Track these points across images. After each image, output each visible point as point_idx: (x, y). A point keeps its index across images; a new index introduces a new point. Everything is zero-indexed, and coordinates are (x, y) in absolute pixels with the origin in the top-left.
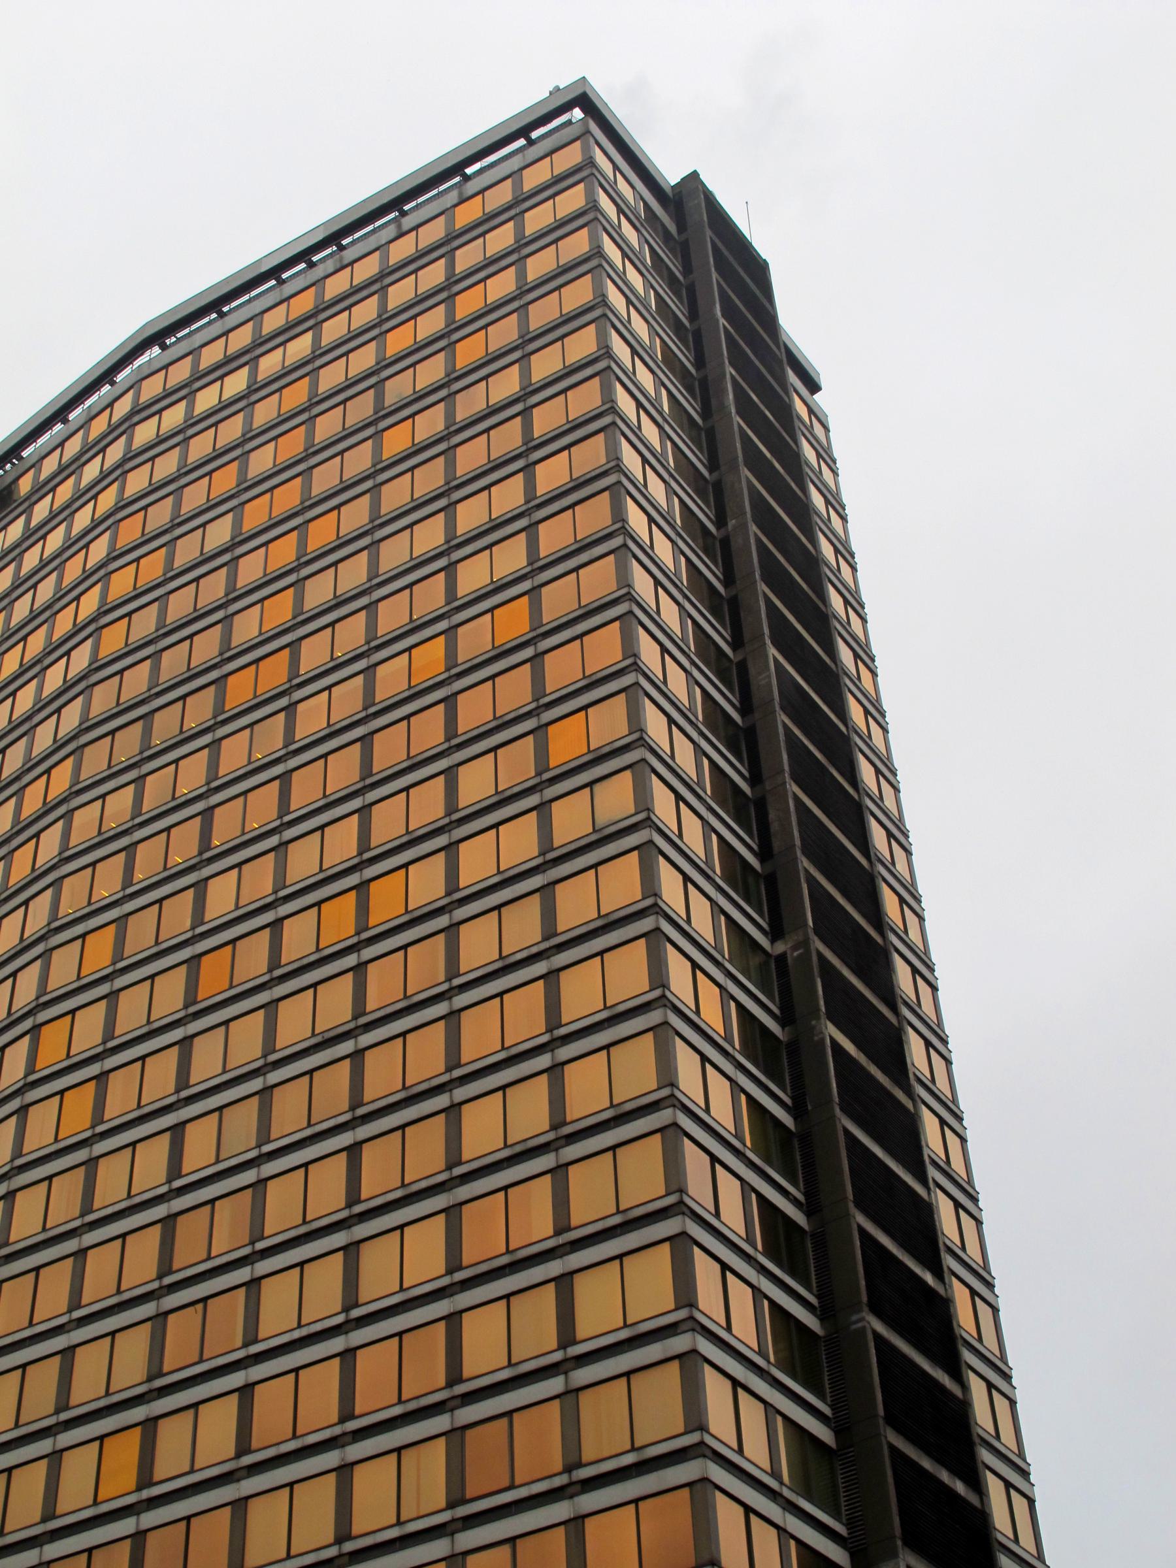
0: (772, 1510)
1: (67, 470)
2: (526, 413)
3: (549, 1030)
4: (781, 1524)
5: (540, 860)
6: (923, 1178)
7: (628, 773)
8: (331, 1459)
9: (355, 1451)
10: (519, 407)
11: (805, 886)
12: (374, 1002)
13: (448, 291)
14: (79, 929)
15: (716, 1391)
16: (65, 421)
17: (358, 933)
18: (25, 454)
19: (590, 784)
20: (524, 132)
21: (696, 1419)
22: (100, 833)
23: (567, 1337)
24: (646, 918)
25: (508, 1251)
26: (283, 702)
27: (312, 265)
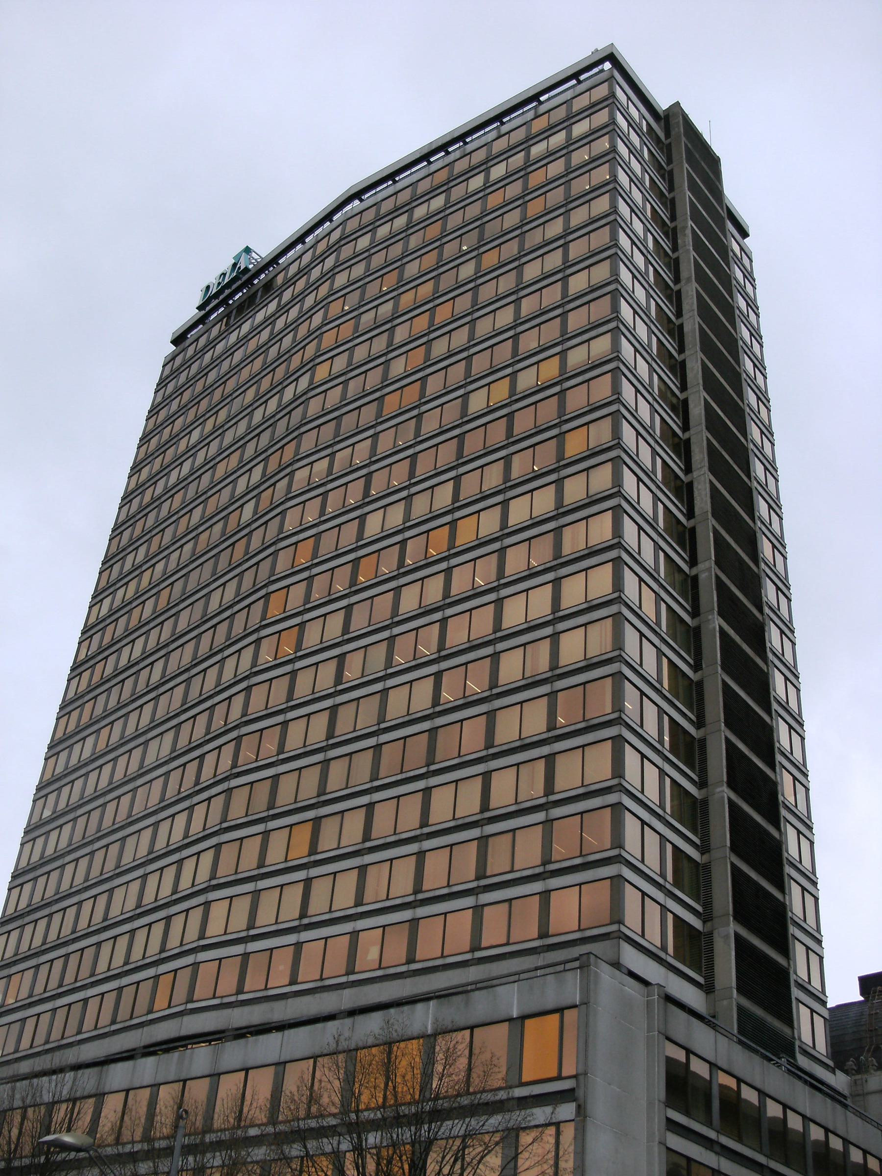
0: (659, 896)
1: (304, 271)
2: (565, 246)
3: (553, 613)
4: (663, 903)
5: (555, 513)
6: (769, 713)
7: (610, 464)
8: (414, 848)
9: (427, 844)
10: (561, 242)
11: (711, 535)
12: (567, 549)
13: (525, 171)
14: (294, 539)
15: (631, 827)
16: (304, 243)
17: (449, 550)
18: (280, 261)
19: (587, 469)
20: (576, 76)
21: (618, 841)
22: (309, 484)
23: (549, 789)
24: (613, 550)
25: (520, 739)
26: (415, 412)
27: (448, 153)
